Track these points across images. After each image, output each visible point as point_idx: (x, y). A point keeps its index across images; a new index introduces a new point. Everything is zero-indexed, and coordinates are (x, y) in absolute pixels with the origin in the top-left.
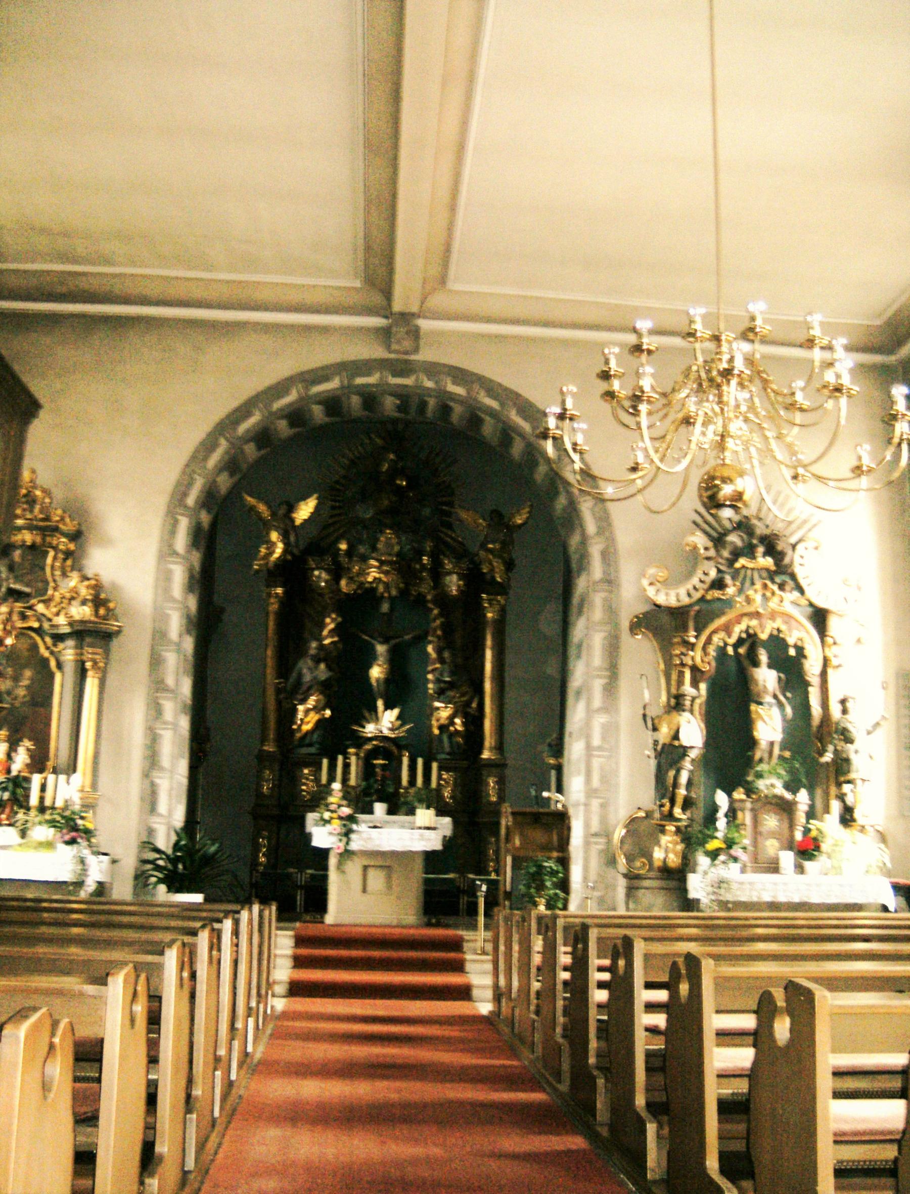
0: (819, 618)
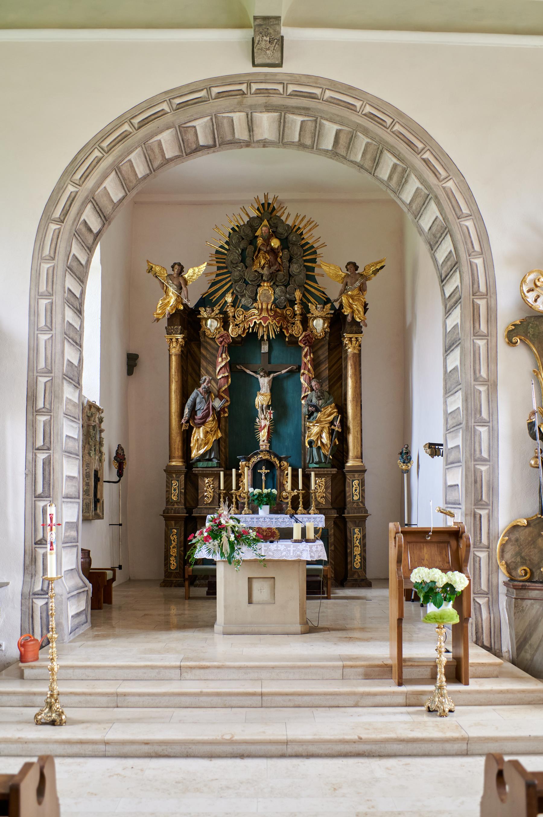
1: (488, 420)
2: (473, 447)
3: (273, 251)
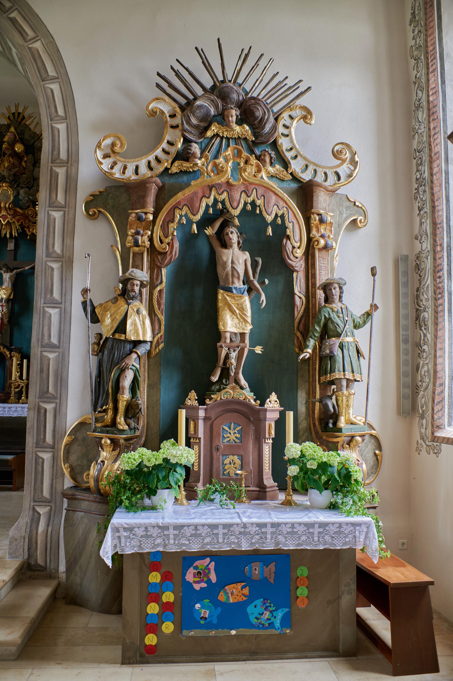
0: (305, 194)
1: (60, 300)
2: (41, 331)
3: (15, 155)
